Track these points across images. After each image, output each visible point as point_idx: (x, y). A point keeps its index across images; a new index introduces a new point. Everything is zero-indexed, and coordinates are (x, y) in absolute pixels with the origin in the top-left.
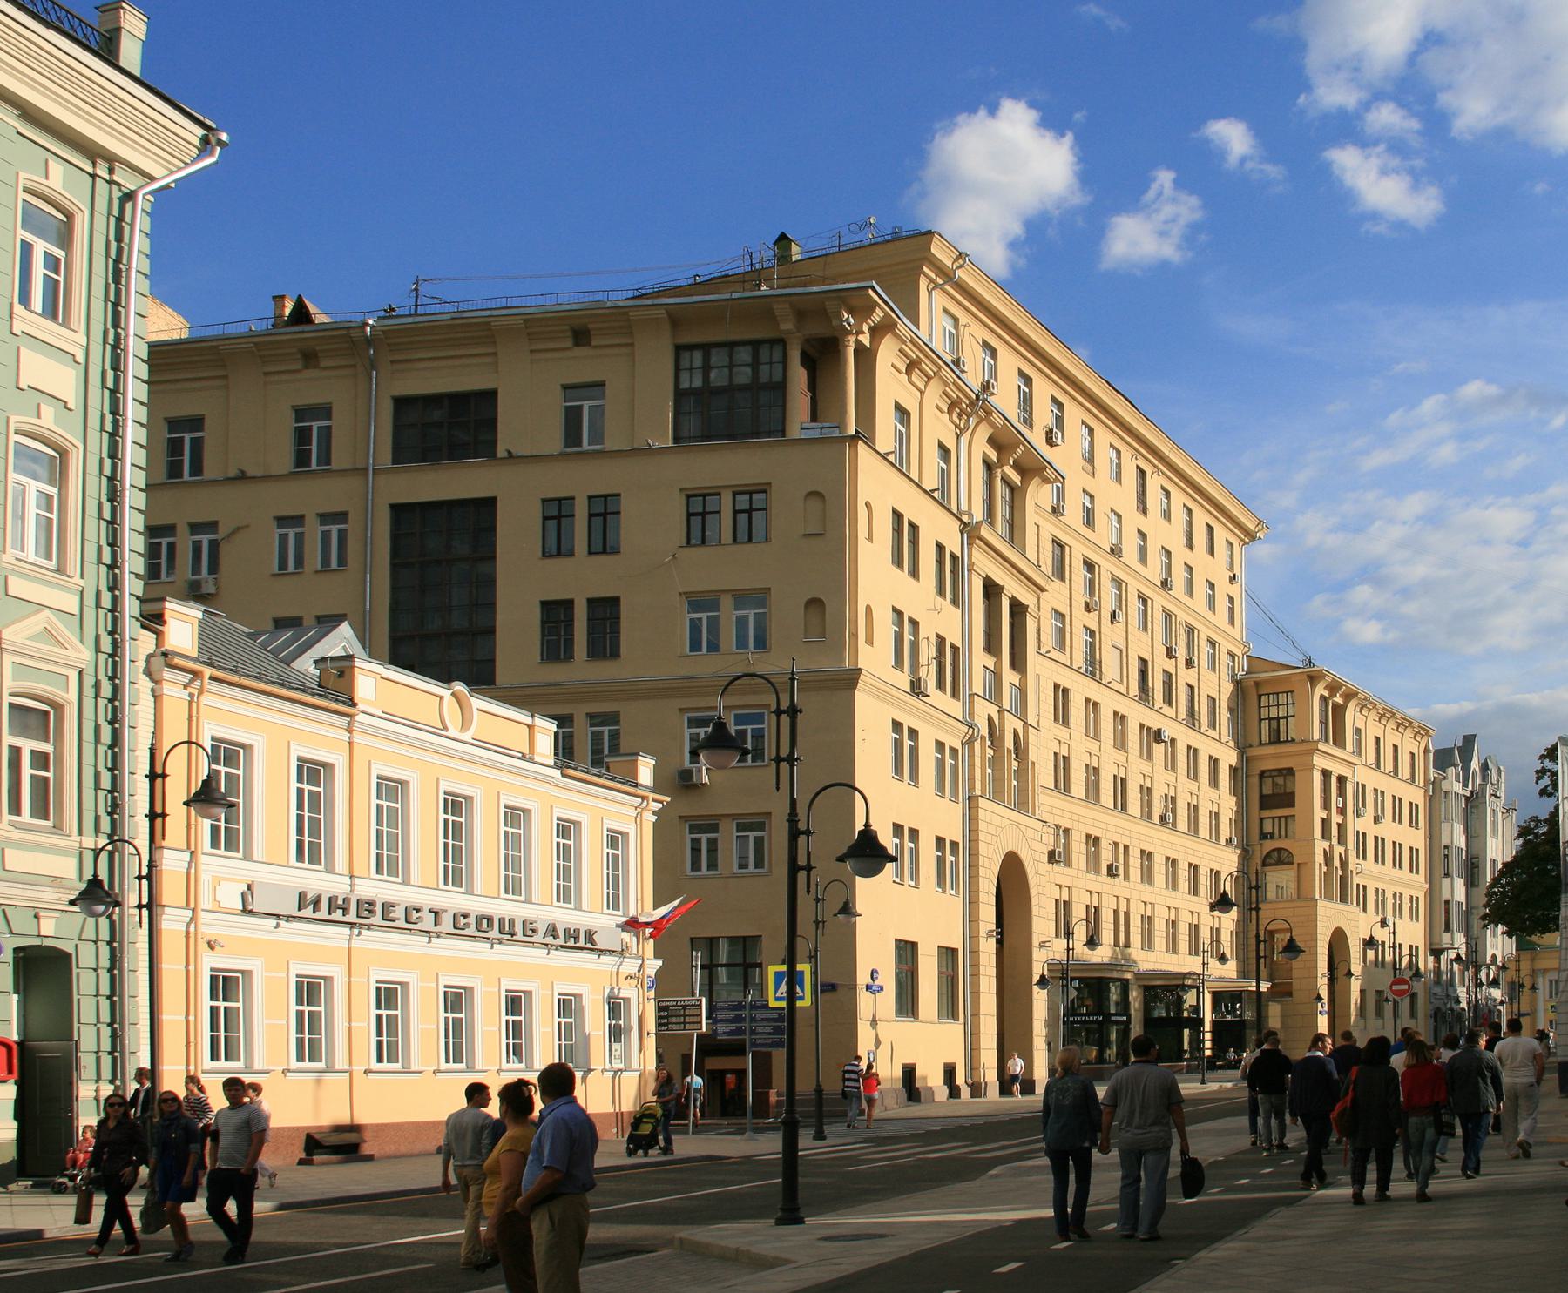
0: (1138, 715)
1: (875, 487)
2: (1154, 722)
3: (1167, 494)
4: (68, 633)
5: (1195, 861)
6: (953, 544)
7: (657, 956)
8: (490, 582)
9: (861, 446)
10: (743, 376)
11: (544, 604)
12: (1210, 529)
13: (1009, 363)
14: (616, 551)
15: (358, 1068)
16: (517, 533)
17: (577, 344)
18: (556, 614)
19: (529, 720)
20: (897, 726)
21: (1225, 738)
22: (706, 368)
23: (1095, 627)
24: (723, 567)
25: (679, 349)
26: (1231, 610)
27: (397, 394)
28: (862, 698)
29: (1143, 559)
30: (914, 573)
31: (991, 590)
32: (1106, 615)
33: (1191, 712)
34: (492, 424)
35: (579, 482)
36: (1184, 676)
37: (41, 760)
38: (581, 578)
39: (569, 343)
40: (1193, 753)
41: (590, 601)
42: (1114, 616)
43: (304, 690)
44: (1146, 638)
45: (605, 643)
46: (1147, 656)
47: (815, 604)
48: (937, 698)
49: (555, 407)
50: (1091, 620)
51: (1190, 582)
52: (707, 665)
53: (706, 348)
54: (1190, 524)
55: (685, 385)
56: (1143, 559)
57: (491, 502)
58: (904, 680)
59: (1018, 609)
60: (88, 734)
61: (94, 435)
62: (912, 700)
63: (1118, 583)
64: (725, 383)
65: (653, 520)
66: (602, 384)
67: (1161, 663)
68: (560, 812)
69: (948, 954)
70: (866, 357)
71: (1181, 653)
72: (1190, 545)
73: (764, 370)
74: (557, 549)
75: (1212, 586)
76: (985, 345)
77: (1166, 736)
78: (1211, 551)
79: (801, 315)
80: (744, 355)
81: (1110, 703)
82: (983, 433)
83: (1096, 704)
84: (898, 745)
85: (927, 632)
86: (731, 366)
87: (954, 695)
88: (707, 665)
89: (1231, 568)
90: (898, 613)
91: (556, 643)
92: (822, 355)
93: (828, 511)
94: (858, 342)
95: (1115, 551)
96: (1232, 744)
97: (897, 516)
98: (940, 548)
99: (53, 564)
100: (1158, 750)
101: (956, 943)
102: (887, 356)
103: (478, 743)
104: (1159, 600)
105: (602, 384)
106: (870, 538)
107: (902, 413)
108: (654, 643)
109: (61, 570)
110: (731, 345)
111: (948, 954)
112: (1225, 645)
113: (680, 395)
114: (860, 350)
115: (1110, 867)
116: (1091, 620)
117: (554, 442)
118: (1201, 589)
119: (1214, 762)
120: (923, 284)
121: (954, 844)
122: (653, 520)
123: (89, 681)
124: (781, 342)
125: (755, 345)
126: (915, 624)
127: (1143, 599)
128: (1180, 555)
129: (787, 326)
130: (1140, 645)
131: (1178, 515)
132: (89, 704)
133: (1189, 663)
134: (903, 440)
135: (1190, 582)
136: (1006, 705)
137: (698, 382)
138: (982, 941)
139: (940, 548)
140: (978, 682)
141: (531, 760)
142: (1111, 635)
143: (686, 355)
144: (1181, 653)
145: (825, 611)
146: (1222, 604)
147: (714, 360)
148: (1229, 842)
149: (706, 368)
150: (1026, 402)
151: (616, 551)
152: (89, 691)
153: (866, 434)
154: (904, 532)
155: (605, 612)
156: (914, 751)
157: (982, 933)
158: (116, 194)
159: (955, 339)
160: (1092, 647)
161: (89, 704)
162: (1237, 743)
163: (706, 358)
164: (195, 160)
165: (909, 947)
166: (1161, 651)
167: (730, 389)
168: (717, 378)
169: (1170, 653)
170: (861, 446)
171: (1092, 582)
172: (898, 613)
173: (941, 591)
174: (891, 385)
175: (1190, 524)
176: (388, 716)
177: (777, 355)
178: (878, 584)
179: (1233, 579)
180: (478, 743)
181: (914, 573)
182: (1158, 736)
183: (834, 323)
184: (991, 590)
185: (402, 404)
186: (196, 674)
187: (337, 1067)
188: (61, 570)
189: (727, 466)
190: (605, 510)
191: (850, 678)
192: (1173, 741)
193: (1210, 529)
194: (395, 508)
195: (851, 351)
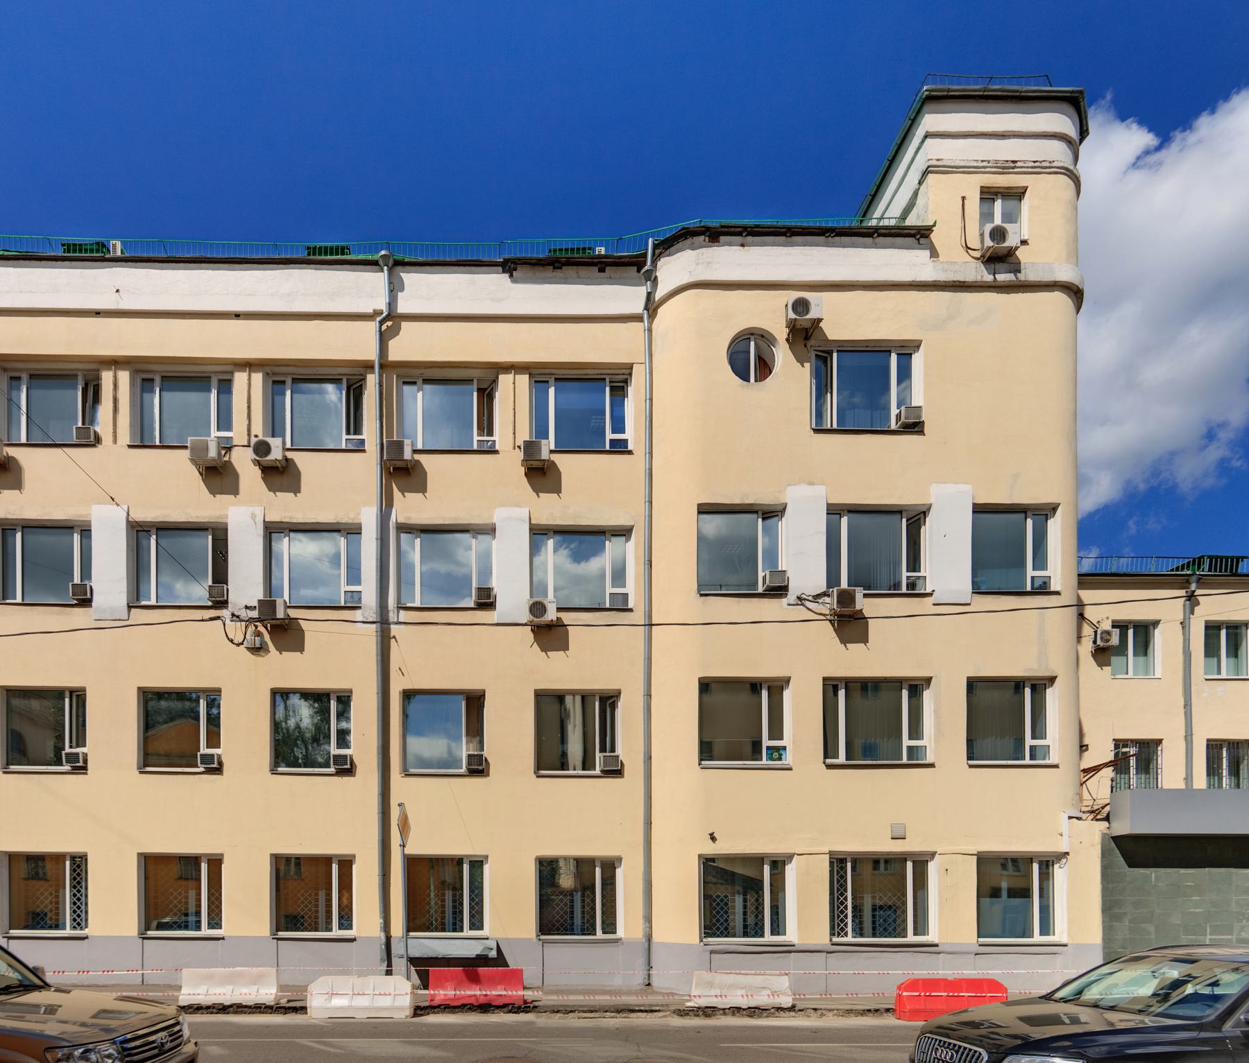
187: (523, 380)
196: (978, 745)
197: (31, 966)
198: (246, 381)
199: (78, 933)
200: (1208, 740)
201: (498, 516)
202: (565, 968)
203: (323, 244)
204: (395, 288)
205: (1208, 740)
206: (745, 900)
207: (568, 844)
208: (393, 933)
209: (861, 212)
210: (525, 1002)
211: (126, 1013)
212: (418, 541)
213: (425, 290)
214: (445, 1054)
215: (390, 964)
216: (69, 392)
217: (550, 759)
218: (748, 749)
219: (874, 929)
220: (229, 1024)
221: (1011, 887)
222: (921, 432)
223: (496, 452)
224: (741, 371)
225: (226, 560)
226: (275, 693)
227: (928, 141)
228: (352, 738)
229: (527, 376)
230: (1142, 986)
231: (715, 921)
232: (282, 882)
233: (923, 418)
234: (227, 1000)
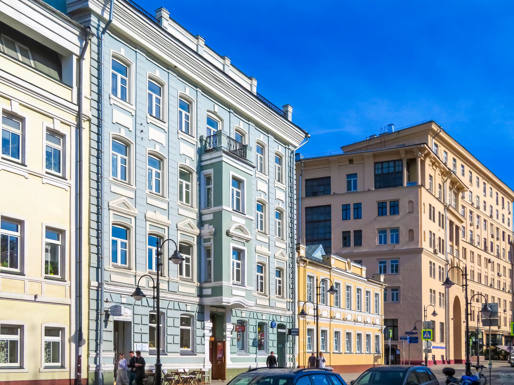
0: (484, 255)
1: (426, 198)
2: (489, 257)
3: (471, 173)
4: (284, 252)
5: (499, 297)
6: (442, 212)
7: (385, 325)
8: (330, 227)
9: (422, 188)
10: (392, 170)
11: (343, 232)
12: (503, 198)
13: (451, 156)
14: (361, 218)
15: (332, 352)
16: (336, 214)
17: (350, 163)
18: (346, 236)
19: (361, 267)
20: (431, 262)
21: (507, 260)
22: (382, 168)
23: (473, 230)
24: (388, 222)
25: (375, 163)
26: (509, 223)
28: (423, 256)
29: (485, 209)
30: (434, 221)
31: (451, 223)
32: (476, 227)
33: (486, 247)
34: (329, 184)
35: (351, 200)
36: (496, 243)
37: (280, 281)
38: (352, 225)
39: (348, 163)
40: (499, 265)
41: (354, 231)
42: (478, 226)
43: (319, 262)
44: (486, 232)
45: (358, 242)
46: (486, 238)
47: (411, 231)
48: (440, 255)
49: (345, 180)
50: (472, 228)
51: (498, 215)
52: (385, 248)
53: (382, 163)
54: (497, 198)
55: (377, 173)
56: (485, 209)
57: (330, 206)
58: (432, 250)
59: (457, 228)
60: (288, 276)
61: (287, 208)
62: (434, 255)
63: (478, 217)
64: (387, 172)
65: (369, 210)
66: (356, 174)
67: (490, 239)
68: (366, 289)
69: (442, 324)
70: (423, 163)
71: (495, 236)
72: (497, 204)
73: (397, 168)
74: (346, 217)
75: (491, 207)
76: (445, 151)
77: (492, 261)
78: (478, 186)
79: (407, 152)
80: (392, 164)
81: (477, 252)
82: (449, 181)
83: (473, 252)
84: (431, 267)
85: (437, 237)
86: (388, 167)
87: (443, 253)
88: (385, 248)
89: (509, 210)
90: (430, 232)
91: (346, 242)
92: (412, 163)
93: (414, 207)
94: (421, 159)
95: (491, 216)
96: (510, 262)
97: (430, 205)
98: (439, 213)
99: (281, 238)
100: (490, 265)
101: (444, 322)
102: (428, 162)
103: (352, 273)
104: (489, 221)
105: (356, 174)
106: (424, 213)
107: (431, 176)
108: (371, 242)
109: (282, 239)
110: (388, 162)
111: (442, 324)
112: (507, 233)
113: (376, 176)
114: (421, 161)
115: (477, 299)
116: (472, 228)
117: (344, 190)
118: (500, 217)
119: (505, 268)
120: (429, 136)
121: (443, 294)
122: (369, 210)
123: (288, 264)
124: (401, 160)
125: (394, 161)
126: (434, 234)
127: (485, 221)
128: (495, 207)
129: (403, 156)
130: (485, 234)
131: (482, 185)
132: (288, 269)
133: (498, 239)
134: (431, 184)
135: (498, 215)
136: (455, 255)
137: (380, 172)
138: (450, 321)
139: (439, 213)
140: (448, 250)
141: (362, 277)
142: (477, 232)
143: (377, 165)
144: (495, 236)
145: (413, 234)
146: (506, 221)
147: (384, 166)
148: (509, 292)
149: (382, 168)
150: (455, 166)
151: (361, 218)
152: (288, 266)
153: (423, 185)
154: (432, 209)
155: (358, 234)
156: (434, 269)
157: (450, 319)
158: (290, 152)
159: (446, 158)
160: (472, 235)
161: (288, 269)
162: (511, 262)
163: (382, 166)
164: (302, 143)
166: (490, 236)
167: (389, 174)
168: (385, 171)
169: (492, 236)
170: (422, 188)
171: (472, 217)
172: (430, 232)
173: (440, 225)
174: (429, 170)
175: (497, 198)
176: (337, 268)
177: (400, 164)
178: (427, 225)
179: (509, 213)
180: (352, 273)
181: (434, 221)
182: (489, 261)
183: (415, 154)
184: (451, 223)
186: (305, 261)
188: (282, 239)
189: (388, 195)
190: (358, 207)
191: (421, 250)
192: (493, 262)
193: (503, 198)
194: (306, 208)
195: (419, 162)
201: (400, 277)
202: (505, 315)
207: (347, 222)
208: (95, 323)
210: (161, 265)
211: (210, 278)
214: (328, 131)
215: (310, 222)
217: (382, 232)
218: (121, 327)
222: (360, 231)
224: (5, 150)
229: (280, 380)
230: (22, 55)
231: (282, 212)
232: (58, 162)
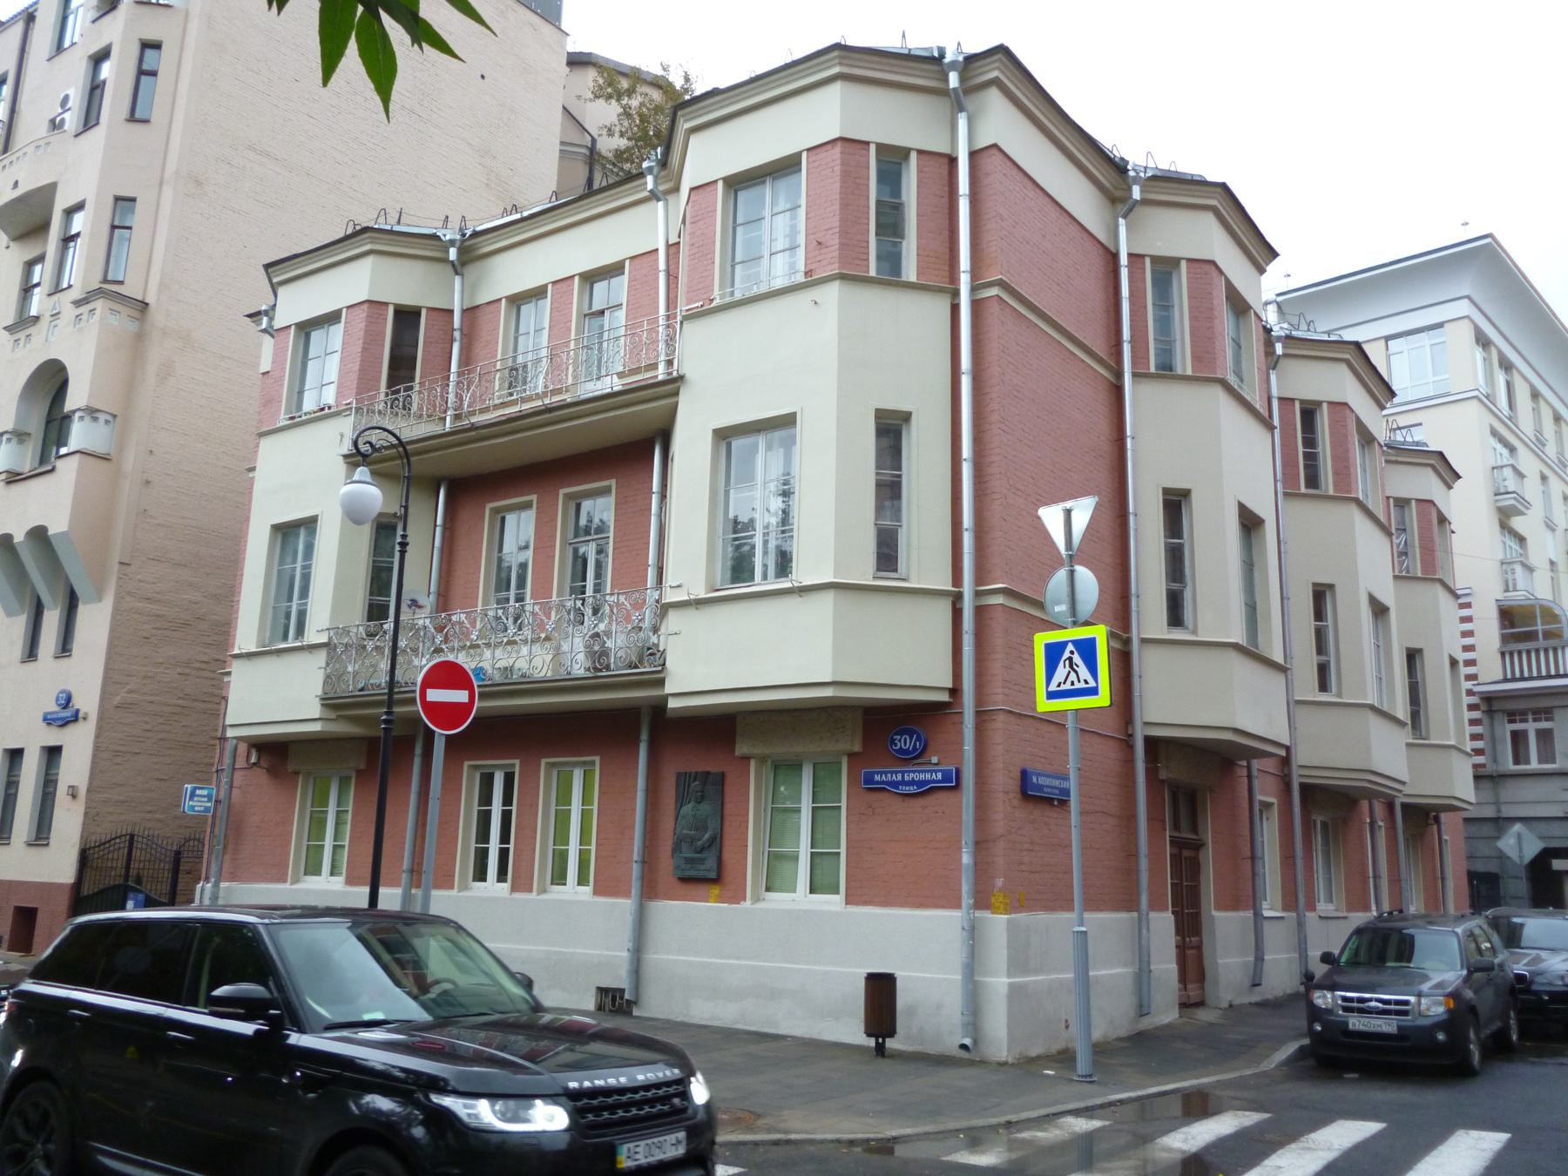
27: (40, 916)
165: (818, 860)
185: (679, 775)
196: (435, 314)
197: (342, 235)
198: (956, 953)
199: (784, 584)
200: (878, 411)
203: (1301, 449)
204: (1499, 811)
205: (878, 411)
206: (391, 459)
209: (285, 596)
212: (625, 954)
213: (78, 809)
216: (1279, 904)
219: (982, 870)
220: (1132, 1090)
221: (193, 795)
223: (249, 316)
225: (1283, 887)
226: (117, 199)
227: (1466, 301)
228: (1559, 746)
229: (620, 1166)
233: (684, 371)
234: (174, 127)
